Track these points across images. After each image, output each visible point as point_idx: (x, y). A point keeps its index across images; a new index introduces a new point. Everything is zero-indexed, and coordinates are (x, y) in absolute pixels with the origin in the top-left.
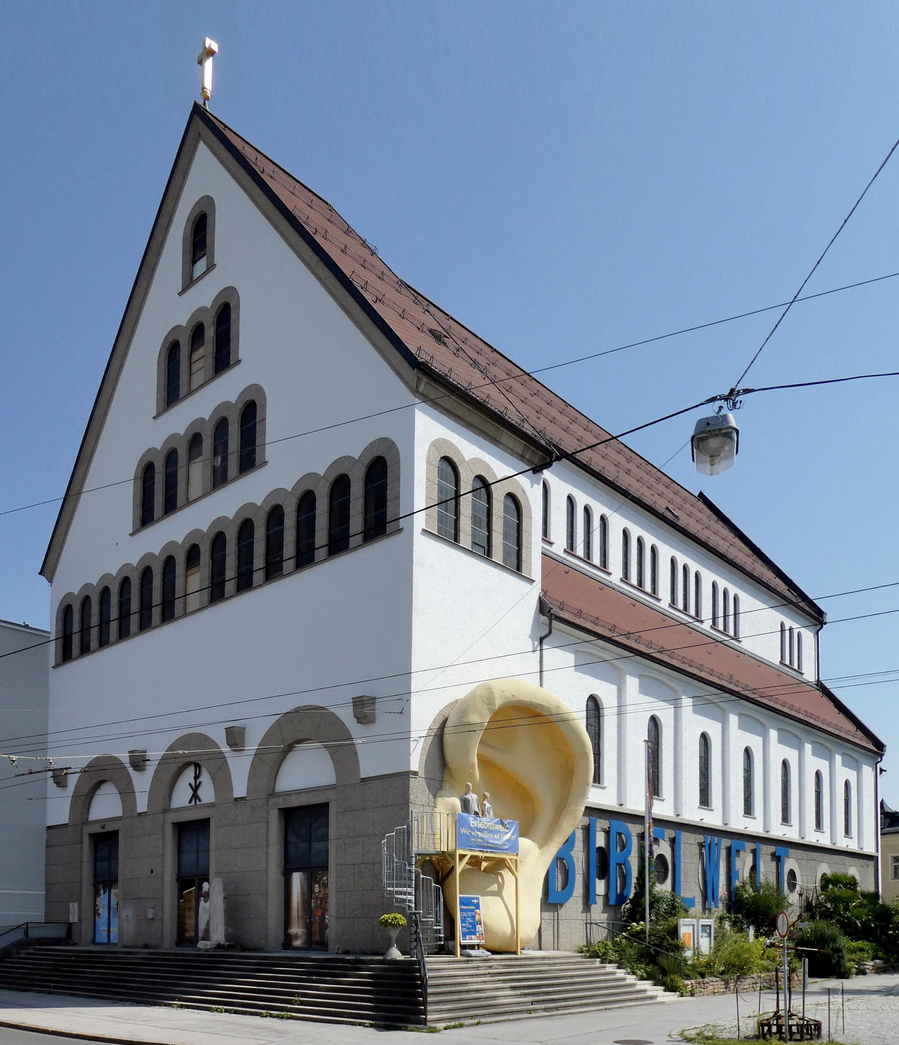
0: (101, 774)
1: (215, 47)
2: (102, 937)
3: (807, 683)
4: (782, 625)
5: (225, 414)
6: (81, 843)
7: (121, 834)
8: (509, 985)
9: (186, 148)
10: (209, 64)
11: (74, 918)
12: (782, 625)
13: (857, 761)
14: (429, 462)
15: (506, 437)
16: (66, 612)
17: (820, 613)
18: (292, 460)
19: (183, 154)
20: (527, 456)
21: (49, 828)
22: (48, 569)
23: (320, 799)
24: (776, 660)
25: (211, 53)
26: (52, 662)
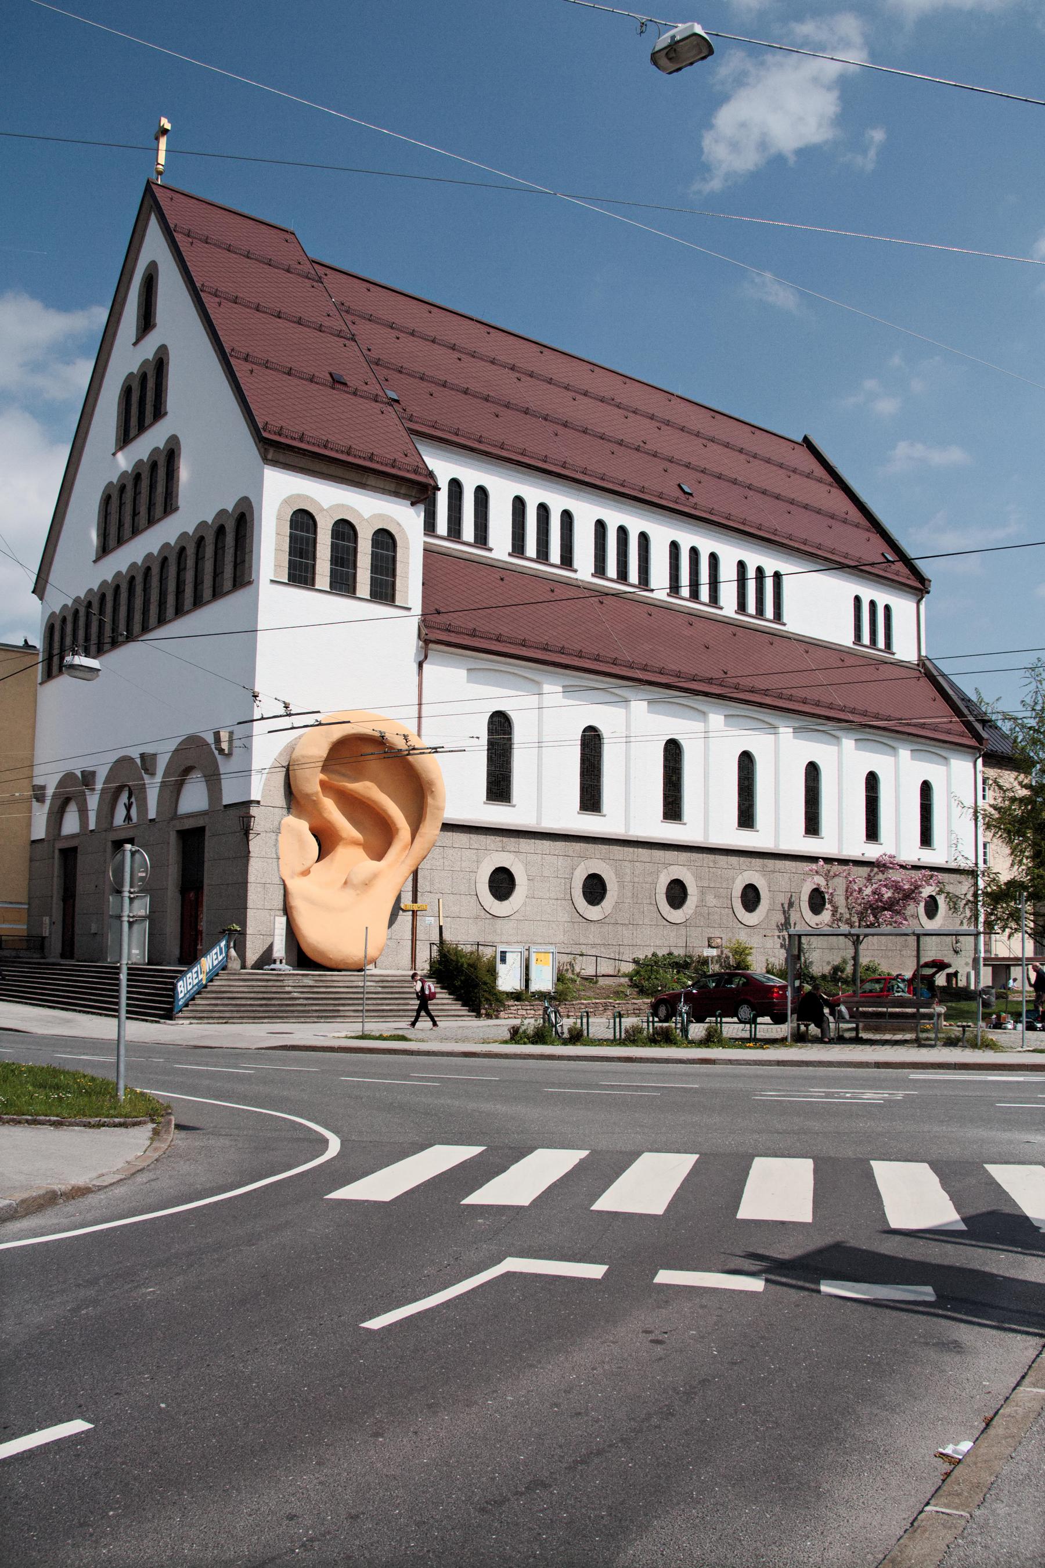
0: (72, 789)
1: (168, 126)
2: (972, 987)
3: (900, 664)
4: (857, 600)
5: (156, 458)
6: (53, 858)
7: (207, 833)
8: (297, 1002)
9: (142, 217)
10: (163, 143)
11: (46, 933)
12: (857, 600)
13: (945, 758)
14: (279, 518)
15: (372, 480)
16: (50, 630)
17: (922, 579)
18: (196, 505)
19: (140, 223)
20: (402, 491)
21: (33, 842)
22: (39, 589)
23: (200, 823)
24: (847, 639)
25: (165, 132)
26: (39, 680)
